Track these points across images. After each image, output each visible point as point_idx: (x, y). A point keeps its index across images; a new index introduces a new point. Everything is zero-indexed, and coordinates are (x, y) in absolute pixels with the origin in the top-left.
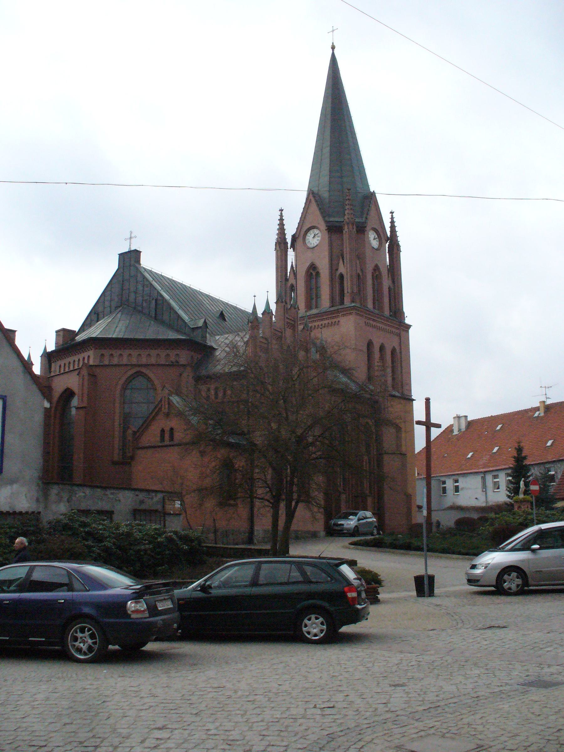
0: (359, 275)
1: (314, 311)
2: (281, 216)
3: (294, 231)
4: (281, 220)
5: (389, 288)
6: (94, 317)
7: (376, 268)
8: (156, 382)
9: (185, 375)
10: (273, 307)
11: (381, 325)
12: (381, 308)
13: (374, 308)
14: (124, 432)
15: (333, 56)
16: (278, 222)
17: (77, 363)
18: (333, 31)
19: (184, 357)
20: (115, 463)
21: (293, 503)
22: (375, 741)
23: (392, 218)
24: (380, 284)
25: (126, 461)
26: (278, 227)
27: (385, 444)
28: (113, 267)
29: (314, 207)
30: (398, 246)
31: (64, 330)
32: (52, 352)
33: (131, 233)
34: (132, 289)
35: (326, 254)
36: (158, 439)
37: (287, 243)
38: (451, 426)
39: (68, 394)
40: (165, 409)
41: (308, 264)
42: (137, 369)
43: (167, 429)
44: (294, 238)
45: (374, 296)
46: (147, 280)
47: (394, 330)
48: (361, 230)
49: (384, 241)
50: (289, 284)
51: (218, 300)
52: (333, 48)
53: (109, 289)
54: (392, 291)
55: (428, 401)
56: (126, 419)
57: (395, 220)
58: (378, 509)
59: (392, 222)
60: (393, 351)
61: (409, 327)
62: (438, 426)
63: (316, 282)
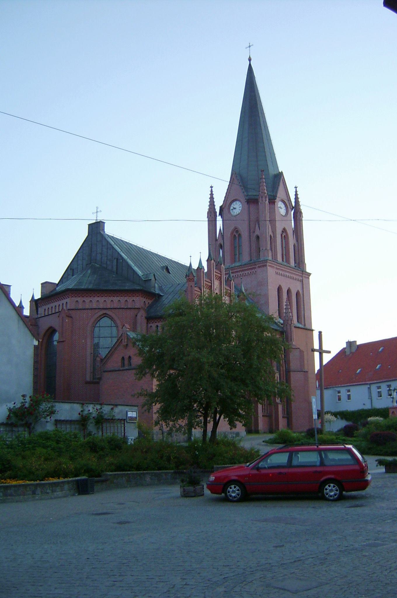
0: (271, 236)
1: (237, 264)
2: (212, 191)
3: (221, 203)
4: (212, 194)
6: (70, 272)
7: (284, 230)
8: (118, 322)
9: (139, 315)
10: (205, 264)
11: (288, 274)
12: (288, 261)
13: (283, 261)
14: (94, 360)
15: (250, 65)
16: (209, 196)
17: (57, 307)
18: (250, 46)
19: (139, 301)
20: (87, 383)
21: (218, 416)
22: (254, 582)
23: (296, 192)
24: (287, 243)
25: (96, 382)
26: (209, 200)
27: (291, 364)
28: (84, 234)
30: (301, 213)
31: (46, 283)
32: (39, 299)
33: (97, 208)
34: (99, 251)
36: (120, 364)
37: (216, 212)
38: (344, 349)
39: (52, 331)
40: (125, 342)
41: (233, 228)
42: (105, 312)
43: (126, 358)
44: (221, 208)
46: (111, 245)
47: (298, 277)
48: (272, 201)
50: (219, 243)
51: (164, 258)
52: (250, 60)
53: (81, 251)
54: (296, 248)
55: (320, 333)
56: (95, 355)
57: (298, 193)
58: (288, 414)
59: (296, 195)
60: (298, 294)
61: (309, 274)
62: (329, 352)
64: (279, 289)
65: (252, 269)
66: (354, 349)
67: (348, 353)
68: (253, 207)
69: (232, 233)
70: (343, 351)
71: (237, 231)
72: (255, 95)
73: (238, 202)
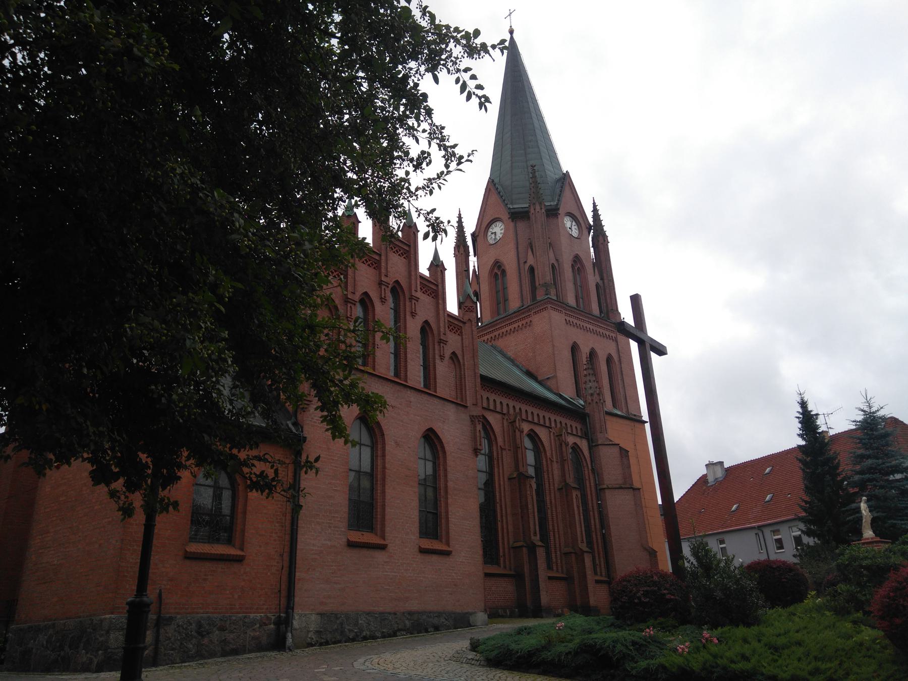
0: (553, 266)
5: (597, 286)
24: (584, 280)
29: (494, 198)
35: (512, 245)
38: (704, 476)
45: (577, 292)
48: (553, 213)
49: (585, 231)
60: (609, 359)
63: (503, 284)
64: (574, 349)
65: (523, 318)
66: (720, 474)
67: (711, 479)
68: (521, 225)
69: (492, 270)
70: (703, 480)
71: (499, 267)
72: (521, 76)
73: (498, 223)
